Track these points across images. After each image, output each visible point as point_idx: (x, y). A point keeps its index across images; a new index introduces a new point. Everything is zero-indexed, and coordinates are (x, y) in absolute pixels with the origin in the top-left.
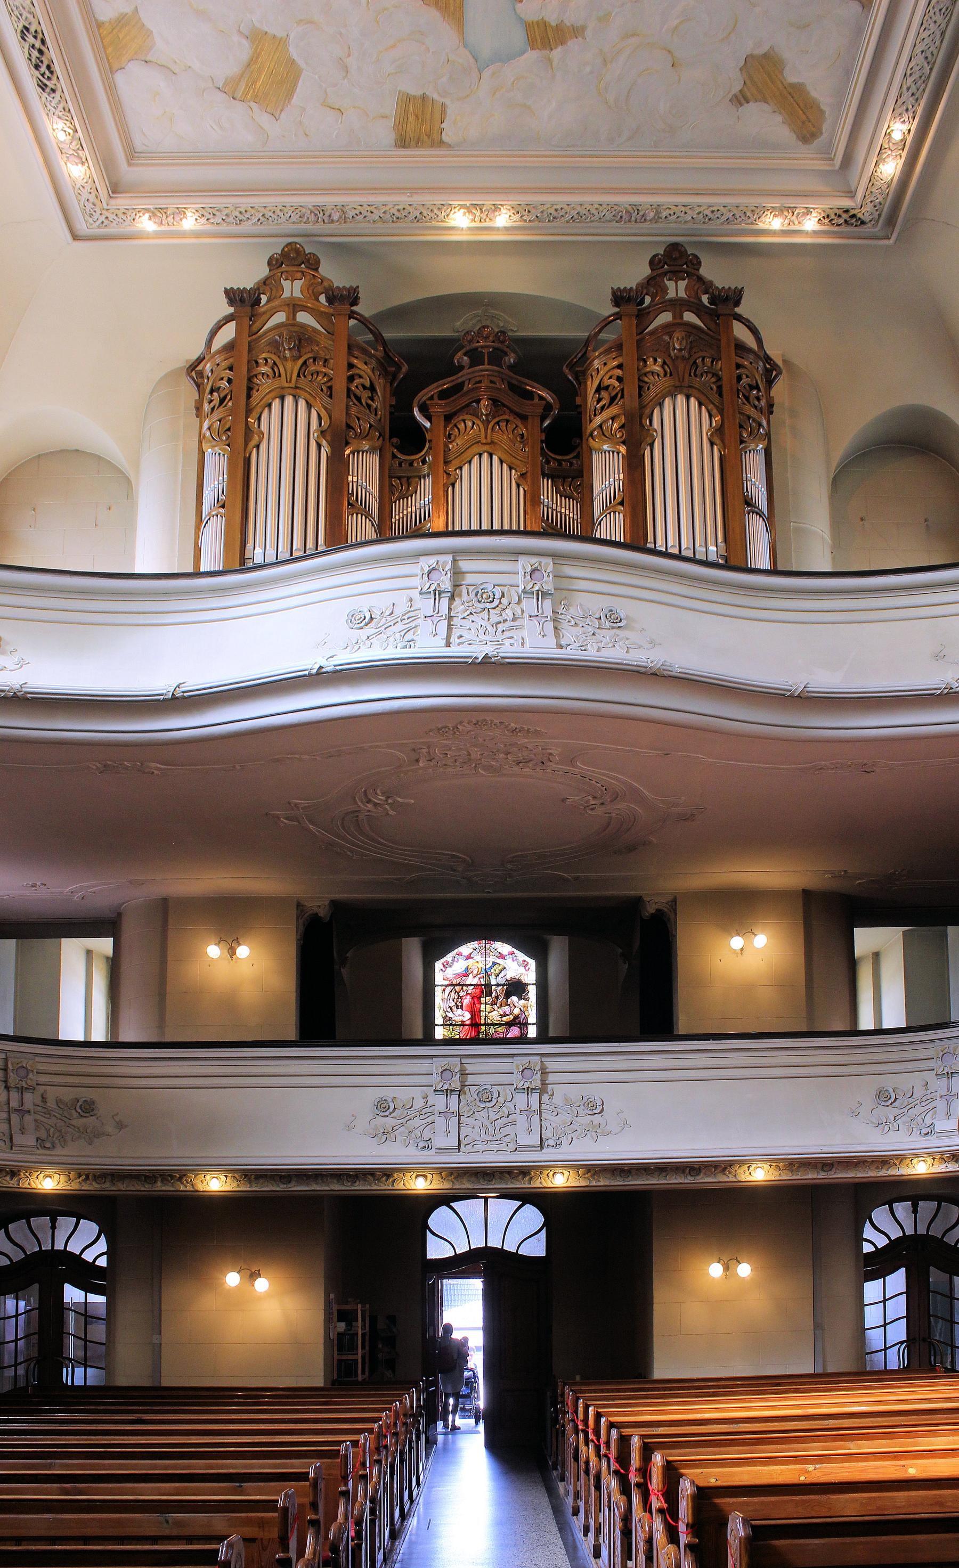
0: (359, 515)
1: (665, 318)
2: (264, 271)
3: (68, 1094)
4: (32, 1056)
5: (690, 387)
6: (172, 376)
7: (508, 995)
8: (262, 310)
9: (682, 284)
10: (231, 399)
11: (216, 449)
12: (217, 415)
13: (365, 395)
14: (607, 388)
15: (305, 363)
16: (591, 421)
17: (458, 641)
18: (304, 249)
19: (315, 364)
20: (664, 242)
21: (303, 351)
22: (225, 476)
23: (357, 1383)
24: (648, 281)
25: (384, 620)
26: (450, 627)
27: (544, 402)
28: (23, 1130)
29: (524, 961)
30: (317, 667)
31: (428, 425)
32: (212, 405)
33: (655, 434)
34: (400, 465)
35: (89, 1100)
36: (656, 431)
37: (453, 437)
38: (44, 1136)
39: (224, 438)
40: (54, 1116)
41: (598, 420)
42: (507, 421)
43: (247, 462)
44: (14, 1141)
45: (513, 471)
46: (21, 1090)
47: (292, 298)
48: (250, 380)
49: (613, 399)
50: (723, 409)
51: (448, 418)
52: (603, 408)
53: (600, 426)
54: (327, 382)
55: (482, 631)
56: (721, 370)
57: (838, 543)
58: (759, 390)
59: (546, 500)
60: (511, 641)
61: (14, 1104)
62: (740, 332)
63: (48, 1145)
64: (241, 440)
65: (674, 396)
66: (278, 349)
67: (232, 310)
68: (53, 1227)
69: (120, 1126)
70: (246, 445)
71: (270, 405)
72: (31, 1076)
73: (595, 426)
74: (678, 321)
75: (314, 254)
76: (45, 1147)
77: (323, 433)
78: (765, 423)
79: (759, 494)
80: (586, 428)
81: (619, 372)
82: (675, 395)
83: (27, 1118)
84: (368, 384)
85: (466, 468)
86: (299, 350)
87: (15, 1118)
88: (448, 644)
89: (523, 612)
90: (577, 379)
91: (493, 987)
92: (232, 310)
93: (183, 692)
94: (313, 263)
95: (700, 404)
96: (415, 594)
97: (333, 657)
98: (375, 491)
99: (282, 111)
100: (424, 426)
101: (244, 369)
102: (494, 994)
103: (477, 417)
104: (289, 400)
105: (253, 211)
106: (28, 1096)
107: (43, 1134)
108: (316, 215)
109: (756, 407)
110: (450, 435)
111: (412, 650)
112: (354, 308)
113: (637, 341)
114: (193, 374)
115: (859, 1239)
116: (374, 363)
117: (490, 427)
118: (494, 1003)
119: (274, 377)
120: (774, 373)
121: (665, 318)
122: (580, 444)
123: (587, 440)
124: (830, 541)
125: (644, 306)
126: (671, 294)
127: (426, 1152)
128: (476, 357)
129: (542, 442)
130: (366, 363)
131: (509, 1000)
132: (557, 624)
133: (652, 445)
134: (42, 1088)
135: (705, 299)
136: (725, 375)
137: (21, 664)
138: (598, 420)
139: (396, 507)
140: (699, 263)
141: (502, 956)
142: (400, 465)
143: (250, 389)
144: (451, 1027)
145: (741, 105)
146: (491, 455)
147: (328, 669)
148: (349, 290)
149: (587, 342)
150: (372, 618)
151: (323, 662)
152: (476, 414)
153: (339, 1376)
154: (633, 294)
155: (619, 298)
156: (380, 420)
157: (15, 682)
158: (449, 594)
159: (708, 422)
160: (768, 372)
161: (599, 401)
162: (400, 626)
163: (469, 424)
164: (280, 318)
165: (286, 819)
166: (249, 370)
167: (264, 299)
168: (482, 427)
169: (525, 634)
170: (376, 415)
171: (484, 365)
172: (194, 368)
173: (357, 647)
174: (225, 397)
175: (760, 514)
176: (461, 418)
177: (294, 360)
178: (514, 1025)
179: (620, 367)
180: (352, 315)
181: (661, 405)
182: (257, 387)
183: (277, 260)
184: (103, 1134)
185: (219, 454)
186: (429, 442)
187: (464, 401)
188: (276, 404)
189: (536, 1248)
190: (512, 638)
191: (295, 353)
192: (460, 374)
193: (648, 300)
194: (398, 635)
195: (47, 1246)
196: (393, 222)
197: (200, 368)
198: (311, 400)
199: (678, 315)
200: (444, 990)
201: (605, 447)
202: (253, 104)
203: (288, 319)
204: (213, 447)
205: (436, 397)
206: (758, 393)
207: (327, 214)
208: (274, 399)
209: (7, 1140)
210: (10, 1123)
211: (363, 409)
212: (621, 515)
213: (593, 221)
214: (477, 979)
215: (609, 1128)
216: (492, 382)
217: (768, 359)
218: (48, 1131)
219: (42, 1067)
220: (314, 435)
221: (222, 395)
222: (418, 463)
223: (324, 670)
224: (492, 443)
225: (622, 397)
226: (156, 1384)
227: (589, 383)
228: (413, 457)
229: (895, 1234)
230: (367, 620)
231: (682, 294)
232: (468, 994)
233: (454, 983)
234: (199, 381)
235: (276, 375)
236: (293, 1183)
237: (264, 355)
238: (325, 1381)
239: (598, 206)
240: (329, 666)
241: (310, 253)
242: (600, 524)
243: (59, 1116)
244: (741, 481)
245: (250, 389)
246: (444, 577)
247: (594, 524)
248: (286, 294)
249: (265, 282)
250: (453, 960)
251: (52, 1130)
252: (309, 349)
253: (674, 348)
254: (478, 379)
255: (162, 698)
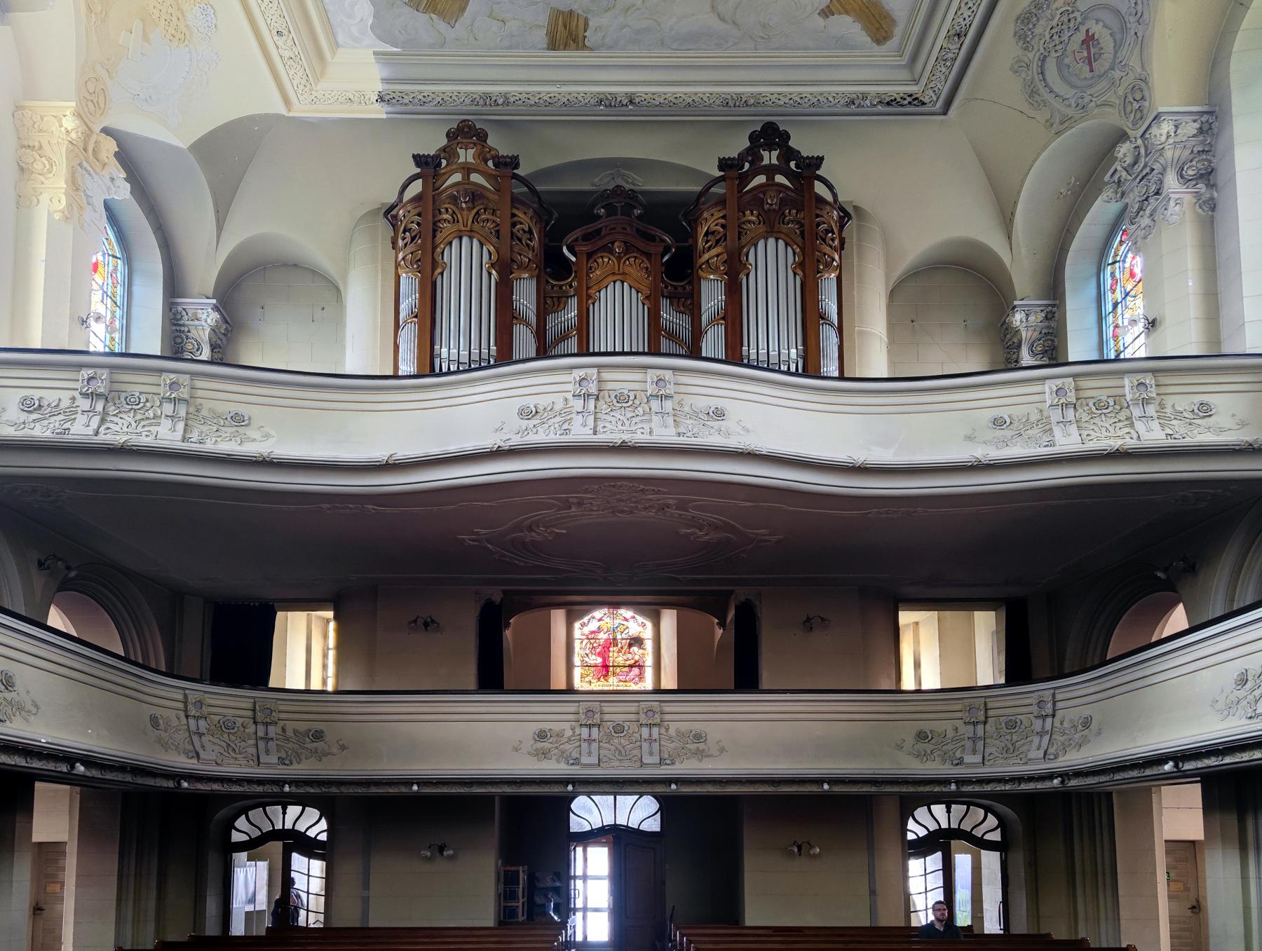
0: (522, 325)
1: (761, 179)
2: (444, 142)
3: (302, 726)
4: (275, 701)
5: (779, 232)
6: (372, 214)
7: (630, 646)
8: (443, 171)
9: (775, 154)
10: (419, 238)
11: (410, 274)
12: (409, 249)
13: (525, 237)
14: (713, 233)
15: (477, 213)
16: (700, 257)
17: (602, 430)
18: (475, 125)
19: (485, 213)
20: (762, 121)
21: (476, 203)
22: (417, 295)
23: (518, 923)
24: (748, 152)
25: (546, 414)
26: (596, 420)
27: (664, 244)
28: (267, 752)
29: (642, 623)
30: (496, 446)
31: (574, 259)
32: (405, 241)
33: (750, 267)
34: (552, 288)
35: (319, 730)
36: (751, 265)
37: (593, 270)
38: (284, 755)
39: (415, 266)
40: (292, 741)
41: (706, 256)
42: (636, 258)
43: (434, 284)
44: (261, 761)
45: (640, 294)
46: (266, 724)
47: (466, 163)
48: (435, 224)
49: (718, 242)
50: (804, 248)
51: (590, 256)
52: (710, 248)
53: (708, 261)
54: (495, 227)
55: (620, 423)
56: (804, 219)
57: (892, 363)
58: (833, 233)
59: (665, 315)
60: (642, 431)
61: (260, 734)
62: (820, 188)
63: (287, 762)
64: (429, 268)
65: (766, 239)
66: (456, 201)
67: (419, 170)
68: (284, 813)
69: (343, 748)
70: (433, 273)
71: (450, 243)
72: (274, 714)
73: (703, 261)
74: (771, 182)
75: (483, 130)
76: (285, 764)
77: (493, 265)
78: (837, 257)
79: (831, 308)
80: (696, 262)
81: (723, 221)
82: (767, 238)
83: (271, 743)
84: (527, 229)
85: (603, 292)
86: (473, 203)
87: (261, 744)
88: (595, 433)
89: (650, 409)
90: (689, 225)
91: (619, 641)
92: (419, 170)
93: (395, 460)
94: (482, 137)
95: (787, 244)
96: (569, 396)
97: (507, 440)
98: (533, 307)
99: (456, 21)
100: (571, 261)
101: (430, 217)
102: (620, 646)
103: (612, 254)
104: (465, 240)
105: (433, 96)
106: (271, 729)
107: (283, 755)
108: (484, 100)
109: (831, 246)
110: (591, 267)
111: (567, 437)
112: (515, 171)
113: (738, 198)
114: (389, 216)
115: (904, 830)
116: (530, 212)
117: (622, 261)
118: (619, 651)
119: (454, 222)
120: (846, 219)
121: (761, 179)
122: (692, 274)
123: (697, 271)
124: (886, 340)
125: (744, 170)
126: (766, 162)
127: (574, 767)
128: (610, 210)
129: (662, 273)
130: (525, 213)
131: (631, 650)
132: (676, 418)
133: (748, 276)
134: (282, 723)
135: (792, 164)
136: (806, 222)
137: (267, 436)
138: (706, 256)
139: (550, 318)
140: (789, 137)
141: (626, 620)
142: (552, 288)
143: (434, 231)
144: (587, 668)
145: (827, 17)
146: (623, 282)
147: (505, 448)
148: (511, 158)
149: (701, 194)
150: (537, 412)
151: (502, 444)
152: (611, 252)
153: (504, 918)
154: (736, 162)
155: (724, 164)
156: (537, 255)
157: (263, 451)
158: (595, 397)
159: (793, 258)
160: (841, 218)
161: (707, 242)
162: (558, 419)
163: (606, 260)
164: (457, 177)
165: (470, 540)
166: (434, 217)
167: (444, 162)
168: (615, 261)
169: (653, 425)
170: (533, 251)
171: (617, 215)
172: (389, 212)
173: (526, 433)
174: (415, 236)
175: (831, 325)
176: (599, 255)
177: (469, 211)
178: (635, 666)
179: (724, 217)
180: (515, 176)
181: (756, 246)
182: (440, 230)
183: (454, 133)
184: (329, 754)
185: (412, 278)
186: (575, 272)
187: (601, 243)
188: (455, 243)
189: (653, 825)
190: (643, 428)
191: (470, 205)
192: (600, 221)
193: (747, 166)
194: (557, 426)
195: (279, 826)
196: (546, 106)
197: (394, 212)
198: (483, 240)
199: (770, 178)
200: (582, 642)
201: (712, 277)
202: (433, 15)
203: (463, 179)
204: (407, 273)
205: (580, 239)
206: (833, 235)
207: (494, 99)
208: (455, 238)
209: (256, 759)
210: (257, 748)
211: (523, 247)
212: (723, 326)
213: (705, 106)
214: (607, 634)
215: (710, 753)
216: (624, 229)
217: (842, 209)
218: (287, 752)
219: (282, 708)
220: (486, 266)
221: (413, 235)
222: (566, 287)
223: (501, 449)
224: (624, 273)
225: (725, 239)
226: (365, 926)
227: (699, 229)
228: (562, 283)
229: (933, 826)
230: (533, 413)
231: (775, 161)
232: (599, 645)
233: (590, 637)
234: (394, 222)
235: (455, 221)
236: (474, 788)
237: (446, 206)
238: (495, 923)
239: (709, 95)
240: (506, 446)
241: (480, 129)
242: (706, 332)
243: (296, 742)
244: (817, 302)
245: (434, 231)
246: (591, 385)
247: (702, 333)
248: (462, 160)
249: (444, 149)
250: (589, 622)
251: (290, 752)
252: (480, 202)
253: (768, 203)
254: (612, 226)
255: (378, 463)
